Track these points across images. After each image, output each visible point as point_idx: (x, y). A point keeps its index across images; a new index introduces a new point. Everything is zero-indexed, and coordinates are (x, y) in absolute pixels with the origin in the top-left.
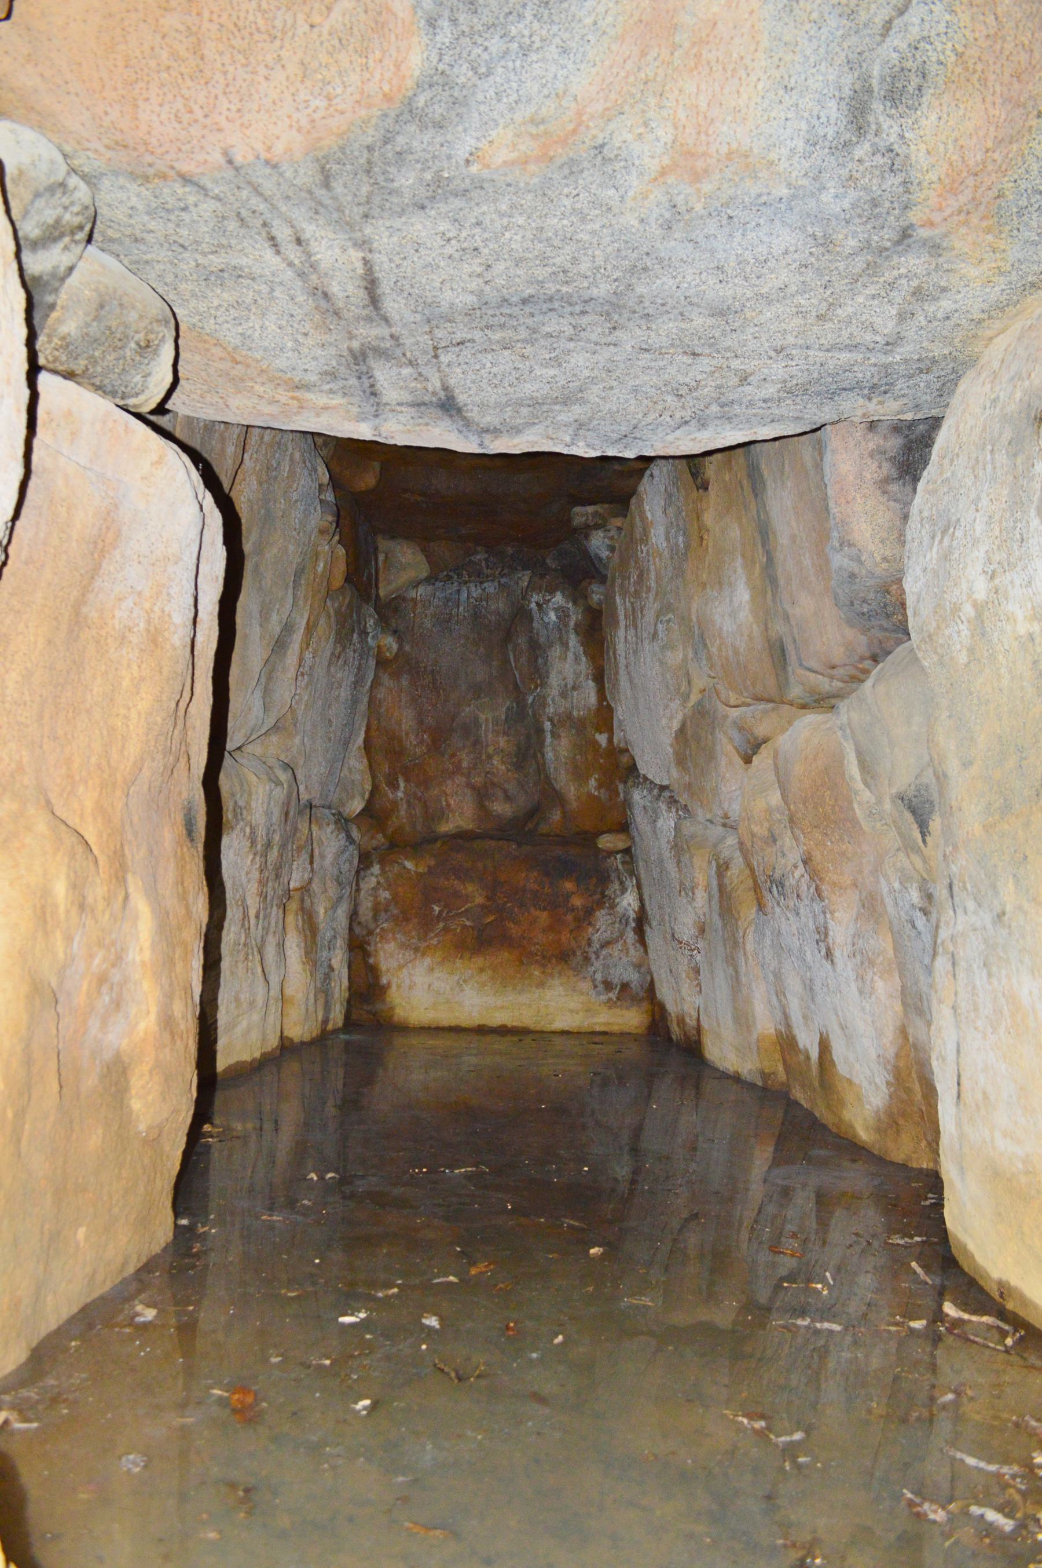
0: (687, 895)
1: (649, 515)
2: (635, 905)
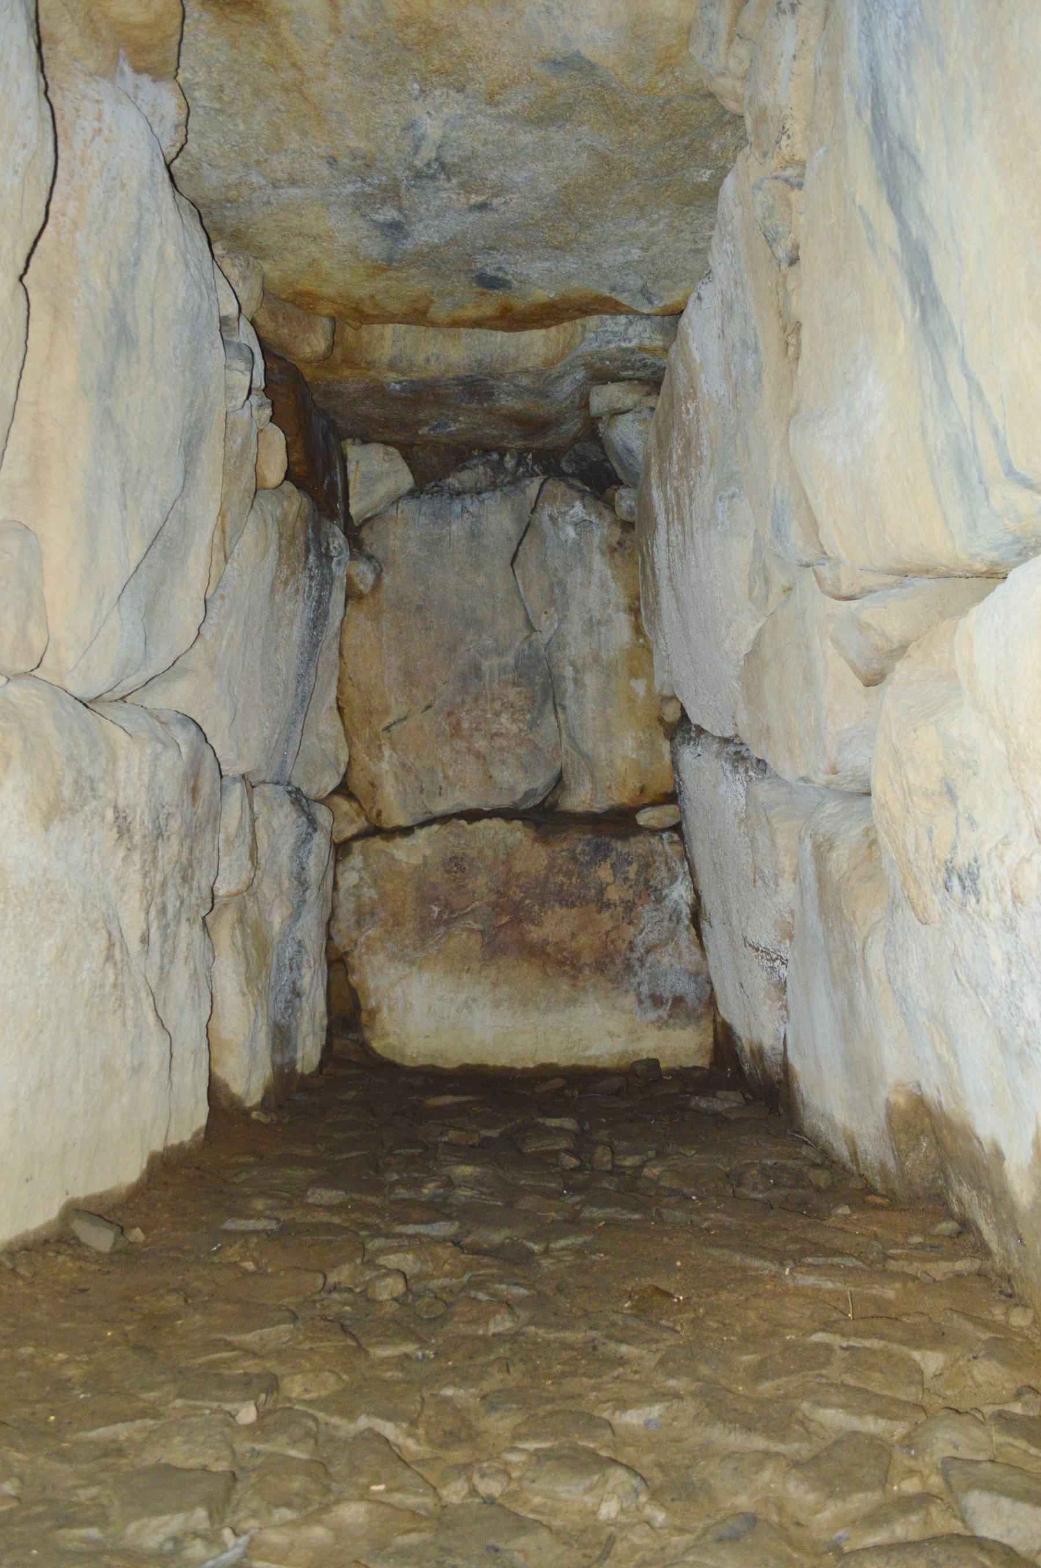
0: (766, 885)
1: (696, 355)
2: (689, 897)
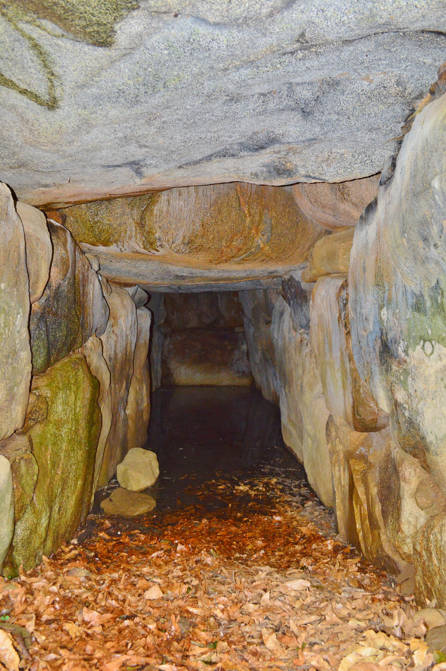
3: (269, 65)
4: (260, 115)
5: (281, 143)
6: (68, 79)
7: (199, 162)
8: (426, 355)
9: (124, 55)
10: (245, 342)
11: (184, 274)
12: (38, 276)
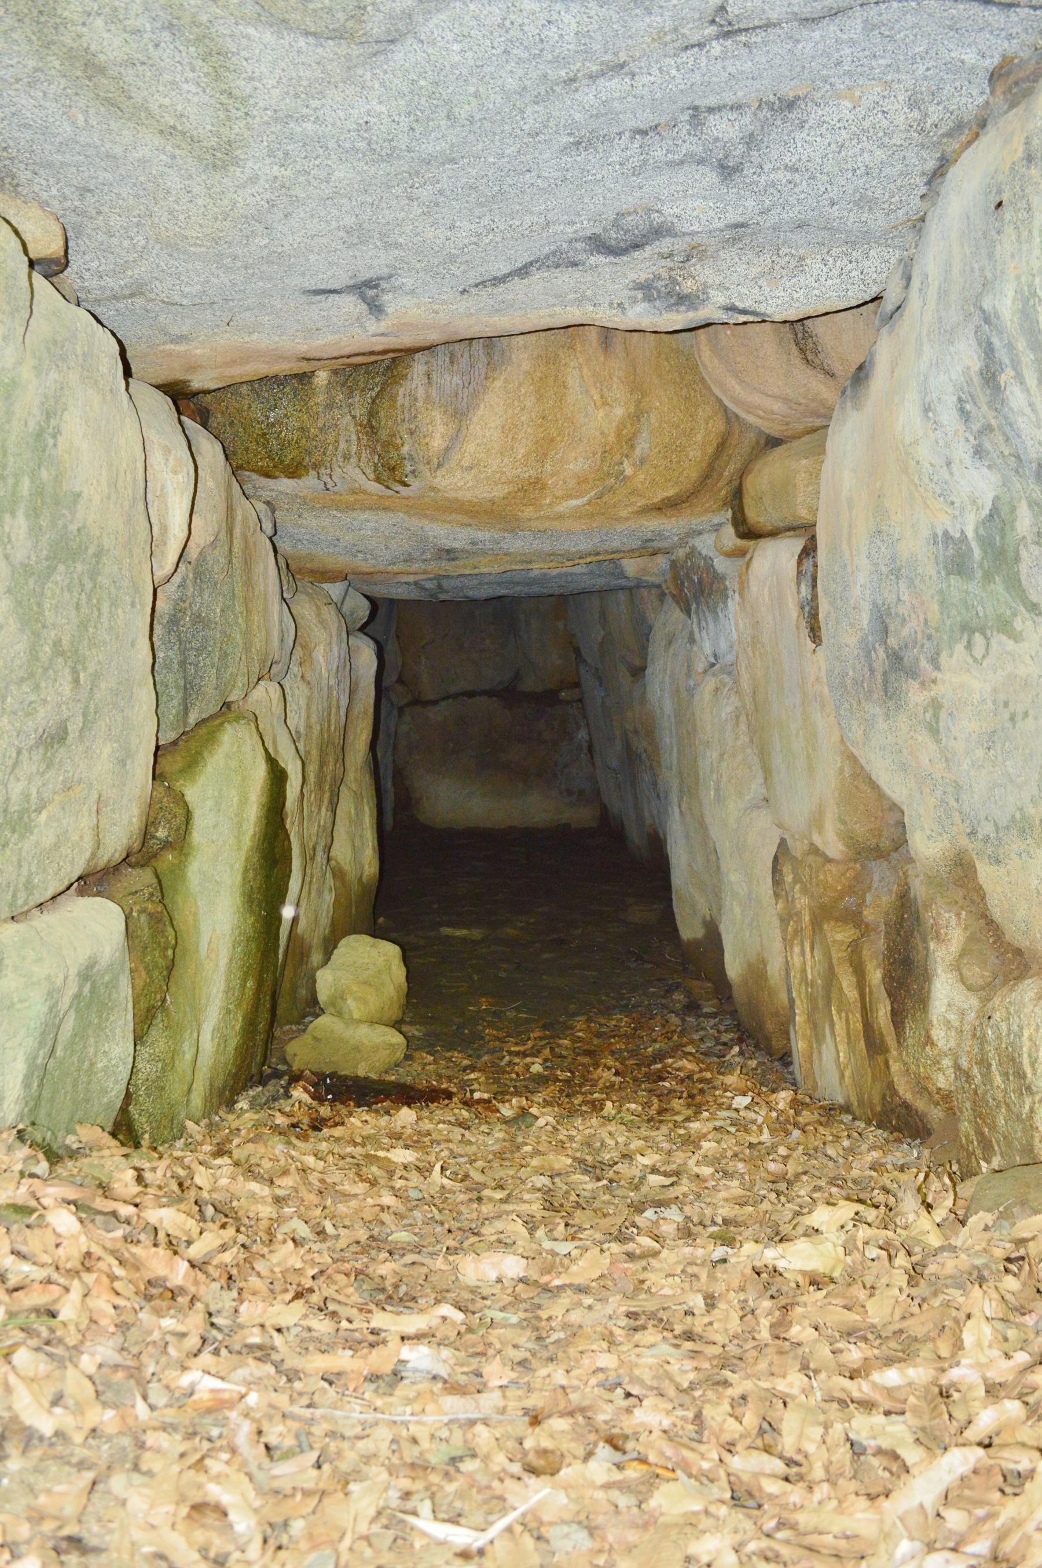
2: (587, 737)
3: (655, 71)
4: (633, 175)
5: (676, 235)
6: (261, 104)
7: (503, 279)
8: (975, 660)
9: (375, 55)
10: (582, 723)
11: (458, 545)
12: (164, 529)
